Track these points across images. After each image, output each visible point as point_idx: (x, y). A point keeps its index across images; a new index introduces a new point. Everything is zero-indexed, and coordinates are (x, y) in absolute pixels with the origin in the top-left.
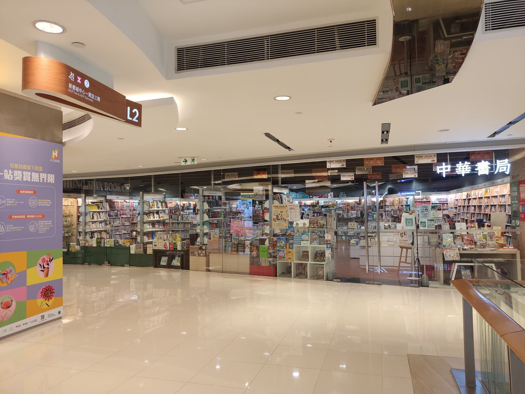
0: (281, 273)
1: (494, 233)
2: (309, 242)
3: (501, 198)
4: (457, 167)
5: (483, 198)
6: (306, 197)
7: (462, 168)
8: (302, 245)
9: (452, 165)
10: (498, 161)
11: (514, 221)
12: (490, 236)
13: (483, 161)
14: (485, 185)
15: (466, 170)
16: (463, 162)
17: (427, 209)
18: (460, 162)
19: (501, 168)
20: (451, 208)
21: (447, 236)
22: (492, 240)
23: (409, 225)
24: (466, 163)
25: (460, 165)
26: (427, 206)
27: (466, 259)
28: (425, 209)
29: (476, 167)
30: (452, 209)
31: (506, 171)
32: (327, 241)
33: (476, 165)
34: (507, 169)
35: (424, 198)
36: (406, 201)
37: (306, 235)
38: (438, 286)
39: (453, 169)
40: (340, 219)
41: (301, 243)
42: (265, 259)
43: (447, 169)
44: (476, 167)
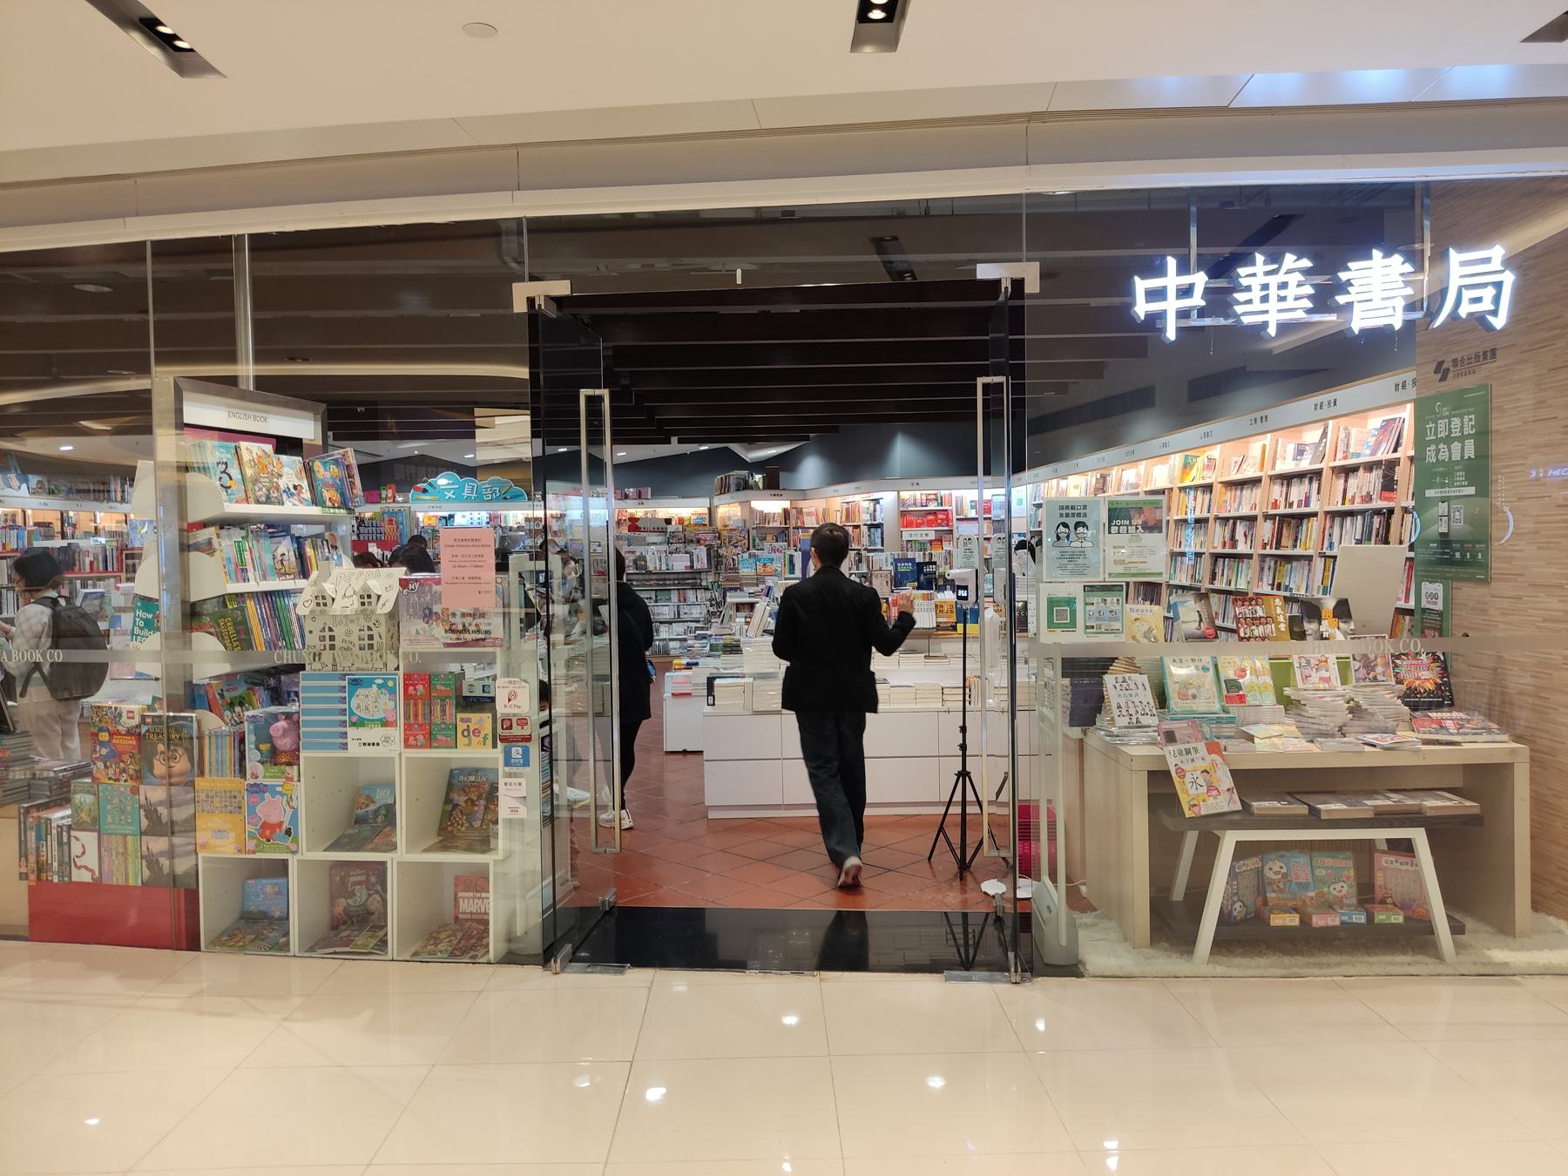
0: (236, 916)
2: (397, 733)
4: (1244, 282)
5: (1265, 481)
7: (1265, 287)
8: (354, 750)
9: (1214, 273)
10: (1455, 257)
11: (1438, 588)
13: (1376, 253)
14: (1207, 435)
15: (1290, 303)
16: (1275, 258)
18: (1259, 258)
19: (1467, 295)
23: (1059, 626)
24: (1289, 260)
25: (1255, 273)
27: (1276, 804)
31: (1495, 313)
32: (508, 723)
33: (1343, 276)
34: (1497, 300)
35: (931, 500)
36: (872, 509)
37: (379, 686)
39: (1219, 300)
40: (667, 577)
41: (349, 741)
42: (125, 844)
43: (1156, 295)
44: (1343, 287)
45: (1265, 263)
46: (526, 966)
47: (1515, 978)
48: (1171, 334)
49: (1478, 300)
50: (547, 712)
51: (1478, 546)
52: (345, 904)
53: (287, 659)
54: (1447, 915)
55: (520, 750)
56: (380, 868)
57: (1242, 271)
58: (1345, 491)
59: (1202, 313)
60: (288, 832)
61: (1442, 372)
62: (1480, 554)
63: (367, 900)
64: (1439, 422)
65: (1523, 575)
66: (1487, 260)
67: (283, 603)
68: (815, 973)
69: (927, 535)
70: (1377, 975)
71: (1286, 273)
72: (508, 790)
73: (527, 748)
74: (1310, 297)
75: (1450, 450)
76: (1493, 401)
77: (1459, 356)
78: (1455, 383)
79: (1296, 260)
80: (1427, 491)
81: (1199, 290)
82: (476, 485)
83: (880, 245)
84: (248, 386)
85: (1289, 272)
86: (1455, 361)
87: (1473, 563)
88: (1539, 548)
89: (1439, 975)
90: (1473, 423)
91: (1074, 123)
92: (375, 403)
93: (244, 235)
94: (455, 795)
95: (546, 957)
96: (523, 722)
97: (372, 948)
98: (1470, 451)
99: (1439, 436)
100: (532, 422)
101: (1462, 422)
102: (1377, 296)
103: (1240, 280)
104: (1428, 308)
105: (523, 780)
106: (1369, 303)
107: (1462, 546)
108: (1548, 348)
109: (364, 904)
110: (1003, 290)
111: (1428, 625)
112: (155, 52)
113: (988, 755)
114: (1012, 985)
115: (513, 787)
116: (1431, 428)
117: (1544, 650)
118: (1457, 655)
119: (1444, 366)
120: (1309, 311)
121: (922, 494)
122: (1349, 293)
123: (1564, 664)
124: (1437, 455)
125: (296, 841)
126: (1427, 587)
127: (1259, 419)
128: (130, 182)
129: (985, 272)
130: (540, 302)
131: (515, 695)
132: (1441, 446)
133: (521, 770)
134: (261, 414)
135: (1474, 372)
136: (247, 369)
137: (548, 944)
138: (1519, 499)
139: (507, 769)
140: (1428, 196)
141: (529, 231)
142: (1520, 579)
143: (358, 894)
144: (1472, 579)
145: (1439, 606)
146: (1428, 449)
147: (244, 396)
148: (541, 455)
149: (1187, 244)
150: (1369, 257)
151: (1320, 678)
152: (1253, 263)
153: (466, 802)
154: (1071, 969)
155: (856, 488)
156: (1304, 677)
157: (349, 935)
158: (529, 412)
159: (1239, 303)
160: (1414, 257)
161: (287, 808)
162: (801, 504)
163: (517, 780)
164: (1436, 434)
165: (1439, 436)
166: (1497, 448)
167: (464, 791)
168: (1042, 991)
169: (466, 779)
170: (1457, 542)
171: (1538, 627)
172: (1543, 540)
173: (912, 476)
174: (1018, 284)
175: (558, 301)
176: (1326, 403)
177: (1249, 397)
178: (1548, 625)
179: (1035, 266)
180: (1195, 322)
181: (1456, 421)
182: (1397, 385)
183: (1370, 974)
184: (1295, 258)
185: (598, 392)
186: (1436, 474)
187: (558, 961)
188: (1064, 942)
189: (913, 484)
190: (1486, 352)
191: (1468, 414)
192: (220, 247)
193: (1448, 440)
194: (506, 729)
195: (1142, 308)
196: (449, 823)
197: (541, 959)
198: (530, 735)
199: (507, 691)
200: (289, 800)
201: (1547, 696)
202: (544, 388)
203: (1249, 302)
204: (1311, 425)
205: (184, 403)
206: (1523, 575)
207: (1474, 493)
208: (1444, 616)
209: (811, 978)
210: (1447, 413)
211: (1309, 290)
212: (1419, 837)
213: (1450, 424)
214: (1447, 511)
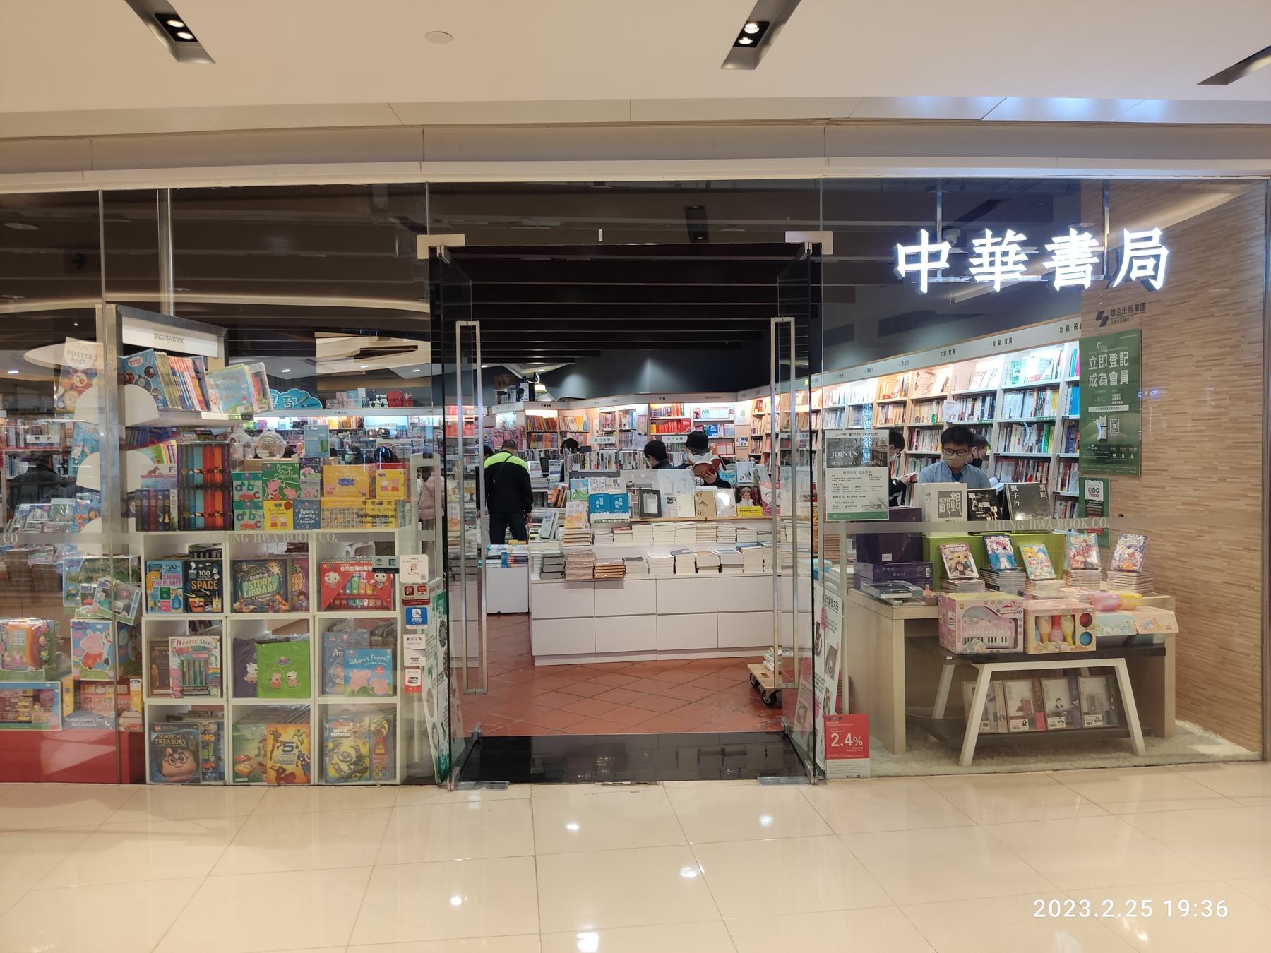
3: (826, 414)
4: (977, 250)
6: (311, 406)
11: (1100, 484)
13: (1073, 231)
14: (905, 363)
15: (1010, 267)
16: (999, 233)
18: (988, 233)
19: (1136, 263)
20: (743, 439)
24: (1010, 234)
25: (985, 244)
30: (745, 442)
31: (1155, 277)
33: (1049, 247)
34: (1156, 268)
38: (891, 767)
39: (959, 263)
45: (993, 236)
47: (1170, 766)
48: (924, 288)
49: (1143, 268)
51: (1130, 449)
53: (1033, 526)
55: (419, 611)
57: (976, 242)
59: (946, 273)
61: (1102, 319)
62: (1132, 455)
65: (1166, 471)
66: (1150, 239)
69: (681, 439)
70: (1076, 769)
72: (409, 643)
74: (1024, 263)
77: (1116, 307)
78: (1111, 328)
81: (944, 256)
82: (277, 395)
83: (690, 212)
84: (169, 312)
85: (1010, 243)
86: (1113, 312)
87: (1127, 462)
88: (1178, 451)
90: (1127, 358)
91: (861, 126)
92: (235, 326)
93: (167, 189)
96: (422, 588)
98: (1125, 378)
101: (1118, 357)
104: (1107, 272)
107: (1118, 449)
112: (162, 41)
114: (811, 786)
116: (1093, 362)
117: (1181, 526)
118: (1113, 530)
119: (1104, 315)
120: (1023, 273)
122: (1053, 260)
123: (1198, 536)
124: (1098, 381)
127: (947, 352)
128: (87, 141)
129: (792, 237)
130: (441, 251)
131: (416, 566)
132: (1101, 375)
133: (419, 627)
134: (178, 337)
135: (1128, 320)
136: (168, 297)
140: (1108, 190)
141: (430, 192)
142: (1164, 473)
144: (1126, 474)
145: (1101, 498)
146: (1091, 376)
147: (168, 321)
148: (441, 373)
149: (934, 218)
152: (983, 236)
155: (614, 401)
159: (973, 266)
162: (567, 413)
165: (1100, 367)
170: (1113, 446)
171: (1178, 509)
172: (1182, 445)
173: (661, 395)
174: (817, 248)
175: (451, 250)
177: (936, 335)
179: (830, 234)
180: (940, 279)
181: (1114, 356)
182: (1061, 328)
185: (471, 323)
186: (1099, 395)
187: (453, 780)
190: (1138, 305)
191: (1124, 351)
192: (147, 198)
193: (1107, 371)
195: (903, 268)
198: (429, 599)
199: (410, 563)
201: (1184, 560)
203: (981, 265)
205: (123, 326)
206: (1166, 471)
207: (1128, 410)
208: (1105, 503)
210: (1107, 350)
211: (1024, 257)
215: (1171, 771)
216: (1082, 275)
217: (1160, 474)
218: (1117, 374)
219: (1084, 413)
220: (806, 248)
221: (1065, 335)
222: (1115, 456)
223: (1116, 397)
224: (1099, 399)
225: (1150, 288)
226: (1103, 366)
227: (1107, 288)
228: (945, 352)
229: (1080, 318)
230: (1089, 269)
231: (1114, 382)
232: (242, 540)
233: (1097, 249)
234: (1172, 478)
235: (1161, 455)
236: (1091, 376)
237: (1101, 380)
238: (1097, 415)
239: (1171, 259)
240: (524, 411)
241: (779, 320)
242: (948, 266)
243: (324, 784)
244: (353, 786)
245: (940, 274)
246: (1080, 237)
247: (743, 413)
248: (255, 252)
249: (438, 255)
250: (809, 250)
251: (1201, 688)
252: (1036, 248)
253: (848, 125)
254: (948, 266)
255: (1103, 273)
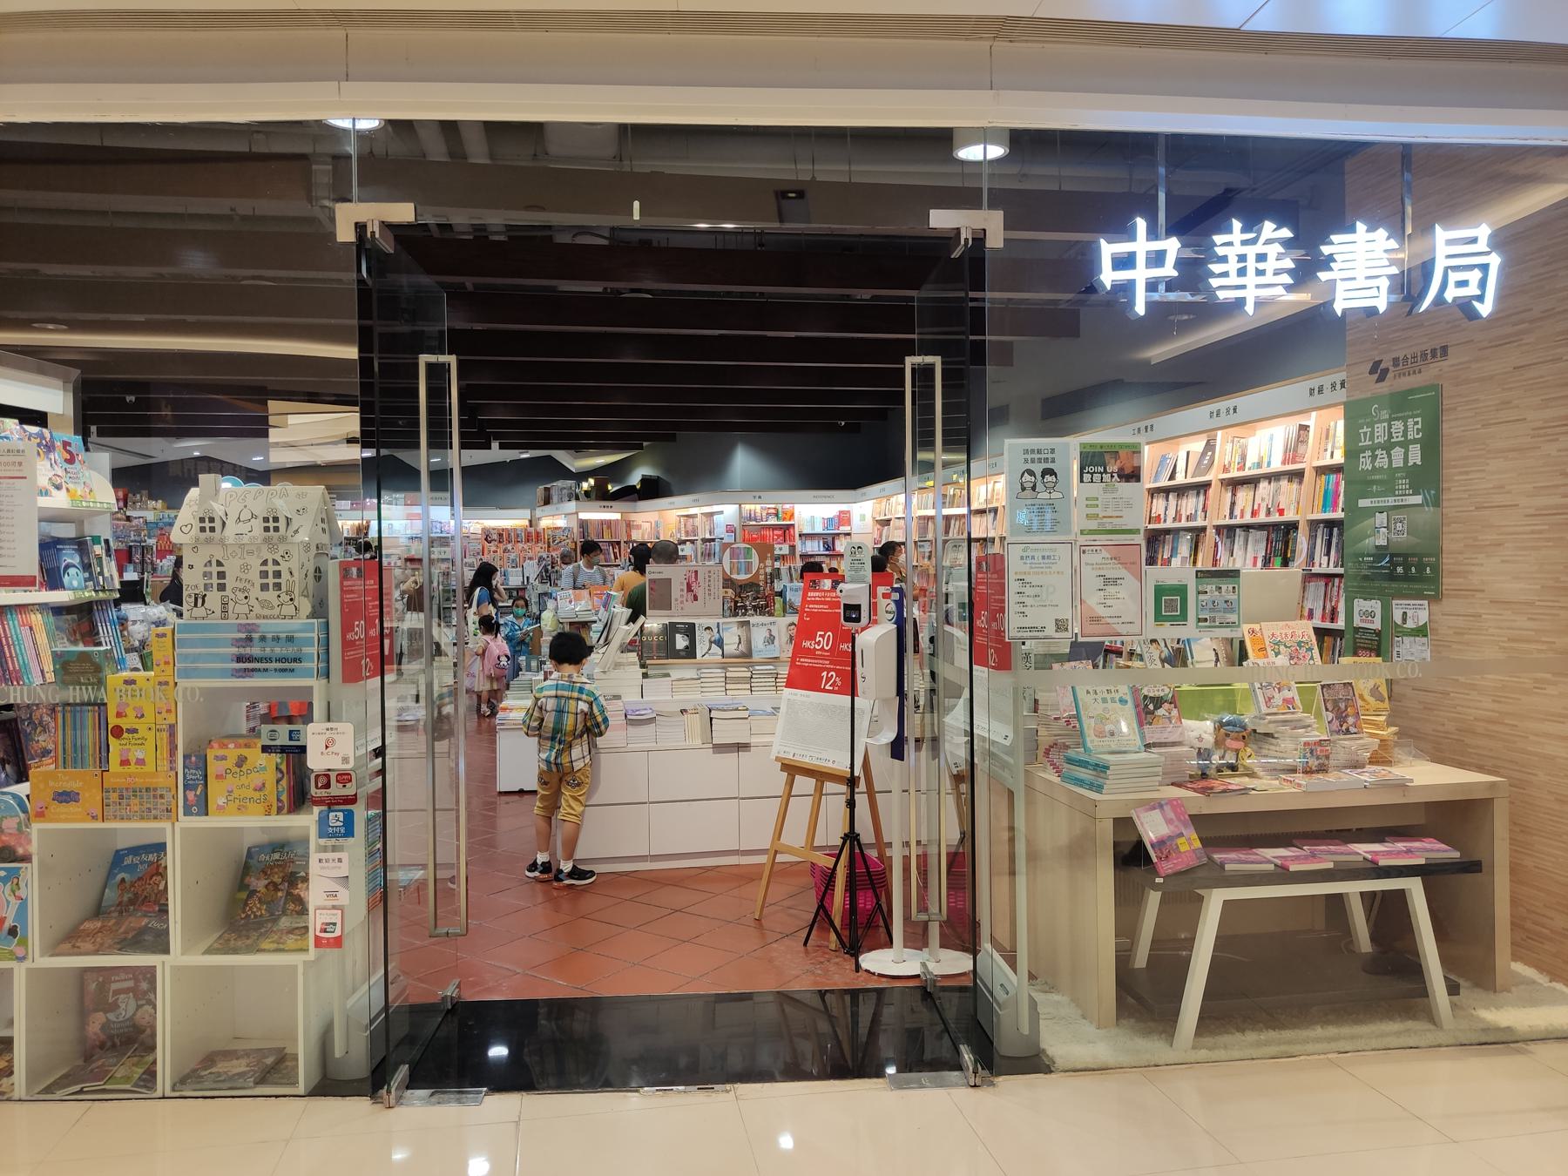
1: (1350, 684)
4: (1220, 251)
11: (1375, 605)
12: (1336, 702)
13: (1361, 227)
16: (1251, 224)
17: (1051, 472)
18: (1237, 225)
19: (1454, 277)
21: (1099, 697)
22: (1348, 732)
24: (1268, 227)
25: (1231, 241)
26: (1053, 451)
28: (1038, 468)
29: (1329, 260)
31: (1480, 298)
33: (1326, 250)
34: (1483, 284)
39: (1193, 272)
45: (1244, 230)
46: (348, 1098)
48: (1140, 309)
49: (1462, 284)
50: (380, 760)
52: (104, 1020)
54: (1445, 977)
55: (341, 815)
56: (149, 974)
57: (1218, 239)
58: (1233, 504)
59: (1171, 285)
60: (13, 932)
63: (134, 1014)
64: (1376, 426)
66: (1474, 240)
67: (27, 620)
68: (728, 1086)
71: (1264, 244)
72: (322, 868)
73: (351, 813)
74: (1289, 271)
75: (1389, 456)
76: (1444, 403)
79: (1275, 230)
80: (1360, 501)
81: (1171, 259)
85: (1269, 242)
86: (1396, 361)
87: (1420, 578)
89: (1439, 1046)
94: (253, 879)
95: (374, 1083)
96: (344, 778)
97: (136, 1085)
98: (1415, 456)
99: (1376, 442)
100: (362, 419)
101: (1406, 426)
102: (1360, 274)
103: (1215, 248)
105: (344, 855)
106: (1353, 281)
108: (1516, 344)
109: (131, 1018)
110: (962, 242)
111: (1362, 645)
113: (890, 792)
115: (331, 864)
116: (1365, 433)
119: (1383, 366)
120: (1289, 288)
121: (762, 508)
125: (24, 943)
126: (1360, 605)
130: (374, 228)
135: (1420, 372)
137: (379, 1059)
138: (1476, 508)
139: (322, 841)
143: (123, 1006)
145: (1377, 624)
146: (1362, 455)
150: (1352, 230)
151: (1284, 700)
153: (266, 887)
154: (1033, 1063)
156: (1267, 699)
157: (103, 1065)
158: (357, 409)
159: (1213, 275)
160: (1398, 232)
161: (12, 899)
162: (633, 517)
163: (336, 855)
164: (1372, 438)
165: (1376, 442)
166: (1448, 454)
167: (266, 874)
168: (1012, 1090)
169: (267, 858)
173: (753, 489)
174: (979, 239)
175: (395, 229)
176: (1223, 411)
178: (1515, 645)
180: (1161, 295)
181: (1398, 426)
183: (1366, 1048)
184: (1275, 226)
185: (443, 358)
187: (393, 1090)
188: (1026, 1030)
189: (755, 497)
190: (1435, 349)
191: (1413, 417)
193: (1388, 447)
194: (321, 788)
195: (1108, 276)
196: (243, 916)
197: (368, 1086)
198: (356, 795)
199: (324, 738)
200: (15, 887)
202: (380, 377)
203: (1225, 274)
204: (1264, 422)
208: (1383, 635)
209: (725, 1094)
212: (1415, 888)
213: (1390, 427)
214: (1385, 521)
215: (1519, 1052)
216: (1374, 292)
217: (1473, 595)
218: (1403, 450)
219: (1350, 507)
220: (963, 237)
221: (1318, 399)
222: (1400, 570)
223: (1403, 484)
224: (1375, 487)
225: (1472, 315)
226: (1381, 440)
227: (1410, 313)
228: (1139, 429)
229: (1345, 373)
230: (1385, 284)
231: (1398, 462)
232: (50, 698)
233: (1394, 256)
234: (1491, 602)
235: (1473, 568)
236: (1362, 455)
237: (1378, 460)
238: (1371, 512)
239: (1502, 268)
240: (577, 513)
241: (918, 359)
242: (1175, 274)
243: (682, 744)
244: (233, 1097)
245: (1162, 287)
246: (1371, 236)
247: (863, 517)
248: (165, 270)
249: (369, 235)
250: (966, 240)
251: (1544, 916)
252: (1303, 252)
253: (1027, 41)
254: (1175, 274)
255: (1403, 292)
